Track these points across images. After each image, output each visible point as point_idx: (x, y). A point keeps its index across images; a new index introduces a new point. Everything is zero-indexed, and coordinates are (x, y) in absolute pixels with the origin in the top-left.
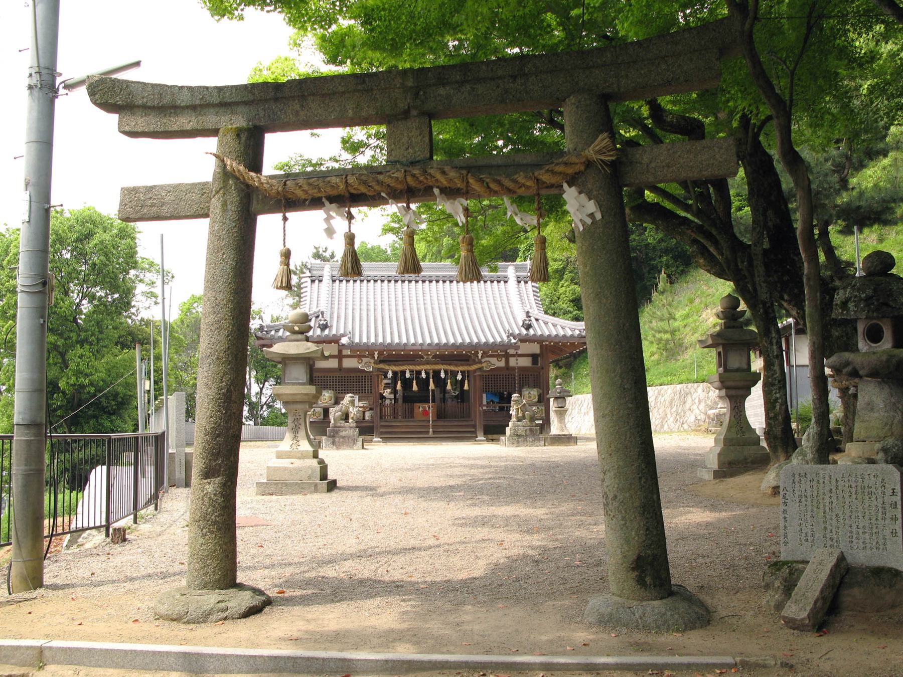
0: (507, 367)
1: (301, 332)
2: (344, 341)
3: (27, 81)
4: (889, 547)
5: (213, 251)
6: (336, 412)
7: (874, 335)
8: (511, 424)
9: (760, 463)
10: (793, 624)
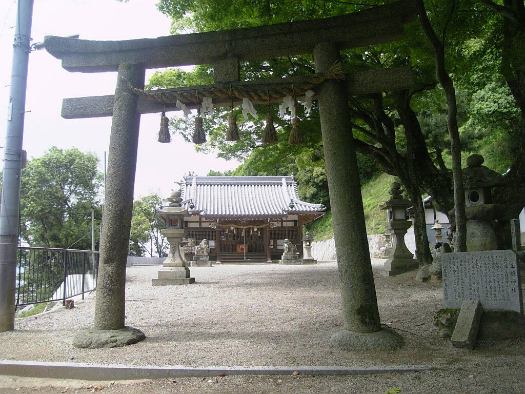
0: (282, 227)
1: (177, 202)
2: (202, 213)
3: (13, 42)
4: (511, 298)
5: (114, 132)
6: (198, 248)
7: (474, 198)
8: (284, 254)
9: (414, 266)
10: (457, 345)
